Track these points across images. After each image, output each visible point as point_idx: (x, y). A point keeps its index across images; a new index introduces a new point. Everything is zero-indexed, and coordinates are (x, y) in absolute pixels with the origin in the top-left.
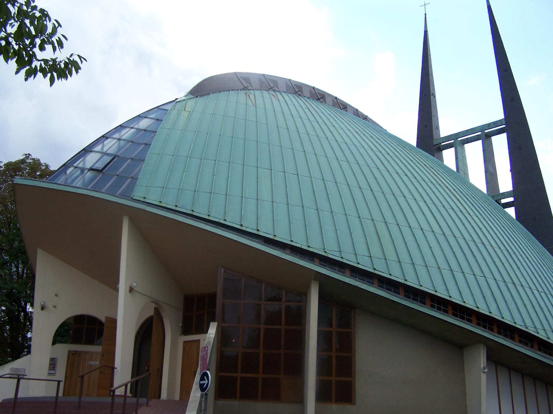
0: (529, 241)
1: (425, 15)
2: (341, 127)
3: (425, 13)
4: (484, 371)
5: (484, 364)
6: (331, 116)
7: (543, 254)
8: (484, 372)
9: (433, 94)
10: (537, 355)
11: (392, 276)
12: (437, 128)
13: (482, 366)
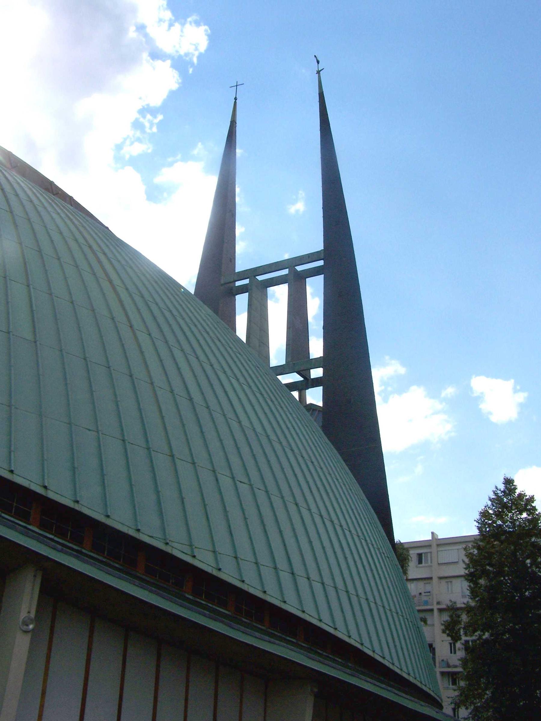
0: (282, 398)
1: (236, 99)
2: (210, 363)
3: (235, 97)
4: (25, 628)
5: (29, 612)
6: (61, 217)
7: (302, 419)
8: (26, 632)
9: (230, 211)
10: (254, 639)
11: (140, 534)
12: (231, 261)
13: (23, 615)
